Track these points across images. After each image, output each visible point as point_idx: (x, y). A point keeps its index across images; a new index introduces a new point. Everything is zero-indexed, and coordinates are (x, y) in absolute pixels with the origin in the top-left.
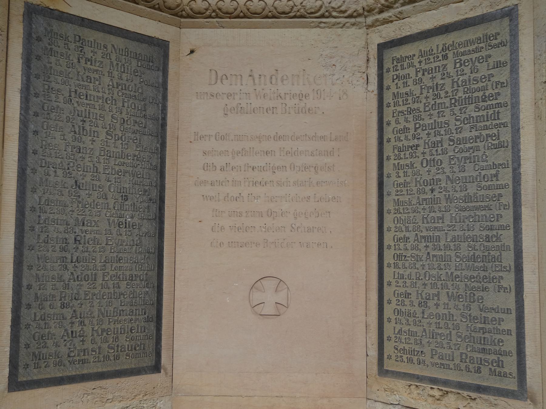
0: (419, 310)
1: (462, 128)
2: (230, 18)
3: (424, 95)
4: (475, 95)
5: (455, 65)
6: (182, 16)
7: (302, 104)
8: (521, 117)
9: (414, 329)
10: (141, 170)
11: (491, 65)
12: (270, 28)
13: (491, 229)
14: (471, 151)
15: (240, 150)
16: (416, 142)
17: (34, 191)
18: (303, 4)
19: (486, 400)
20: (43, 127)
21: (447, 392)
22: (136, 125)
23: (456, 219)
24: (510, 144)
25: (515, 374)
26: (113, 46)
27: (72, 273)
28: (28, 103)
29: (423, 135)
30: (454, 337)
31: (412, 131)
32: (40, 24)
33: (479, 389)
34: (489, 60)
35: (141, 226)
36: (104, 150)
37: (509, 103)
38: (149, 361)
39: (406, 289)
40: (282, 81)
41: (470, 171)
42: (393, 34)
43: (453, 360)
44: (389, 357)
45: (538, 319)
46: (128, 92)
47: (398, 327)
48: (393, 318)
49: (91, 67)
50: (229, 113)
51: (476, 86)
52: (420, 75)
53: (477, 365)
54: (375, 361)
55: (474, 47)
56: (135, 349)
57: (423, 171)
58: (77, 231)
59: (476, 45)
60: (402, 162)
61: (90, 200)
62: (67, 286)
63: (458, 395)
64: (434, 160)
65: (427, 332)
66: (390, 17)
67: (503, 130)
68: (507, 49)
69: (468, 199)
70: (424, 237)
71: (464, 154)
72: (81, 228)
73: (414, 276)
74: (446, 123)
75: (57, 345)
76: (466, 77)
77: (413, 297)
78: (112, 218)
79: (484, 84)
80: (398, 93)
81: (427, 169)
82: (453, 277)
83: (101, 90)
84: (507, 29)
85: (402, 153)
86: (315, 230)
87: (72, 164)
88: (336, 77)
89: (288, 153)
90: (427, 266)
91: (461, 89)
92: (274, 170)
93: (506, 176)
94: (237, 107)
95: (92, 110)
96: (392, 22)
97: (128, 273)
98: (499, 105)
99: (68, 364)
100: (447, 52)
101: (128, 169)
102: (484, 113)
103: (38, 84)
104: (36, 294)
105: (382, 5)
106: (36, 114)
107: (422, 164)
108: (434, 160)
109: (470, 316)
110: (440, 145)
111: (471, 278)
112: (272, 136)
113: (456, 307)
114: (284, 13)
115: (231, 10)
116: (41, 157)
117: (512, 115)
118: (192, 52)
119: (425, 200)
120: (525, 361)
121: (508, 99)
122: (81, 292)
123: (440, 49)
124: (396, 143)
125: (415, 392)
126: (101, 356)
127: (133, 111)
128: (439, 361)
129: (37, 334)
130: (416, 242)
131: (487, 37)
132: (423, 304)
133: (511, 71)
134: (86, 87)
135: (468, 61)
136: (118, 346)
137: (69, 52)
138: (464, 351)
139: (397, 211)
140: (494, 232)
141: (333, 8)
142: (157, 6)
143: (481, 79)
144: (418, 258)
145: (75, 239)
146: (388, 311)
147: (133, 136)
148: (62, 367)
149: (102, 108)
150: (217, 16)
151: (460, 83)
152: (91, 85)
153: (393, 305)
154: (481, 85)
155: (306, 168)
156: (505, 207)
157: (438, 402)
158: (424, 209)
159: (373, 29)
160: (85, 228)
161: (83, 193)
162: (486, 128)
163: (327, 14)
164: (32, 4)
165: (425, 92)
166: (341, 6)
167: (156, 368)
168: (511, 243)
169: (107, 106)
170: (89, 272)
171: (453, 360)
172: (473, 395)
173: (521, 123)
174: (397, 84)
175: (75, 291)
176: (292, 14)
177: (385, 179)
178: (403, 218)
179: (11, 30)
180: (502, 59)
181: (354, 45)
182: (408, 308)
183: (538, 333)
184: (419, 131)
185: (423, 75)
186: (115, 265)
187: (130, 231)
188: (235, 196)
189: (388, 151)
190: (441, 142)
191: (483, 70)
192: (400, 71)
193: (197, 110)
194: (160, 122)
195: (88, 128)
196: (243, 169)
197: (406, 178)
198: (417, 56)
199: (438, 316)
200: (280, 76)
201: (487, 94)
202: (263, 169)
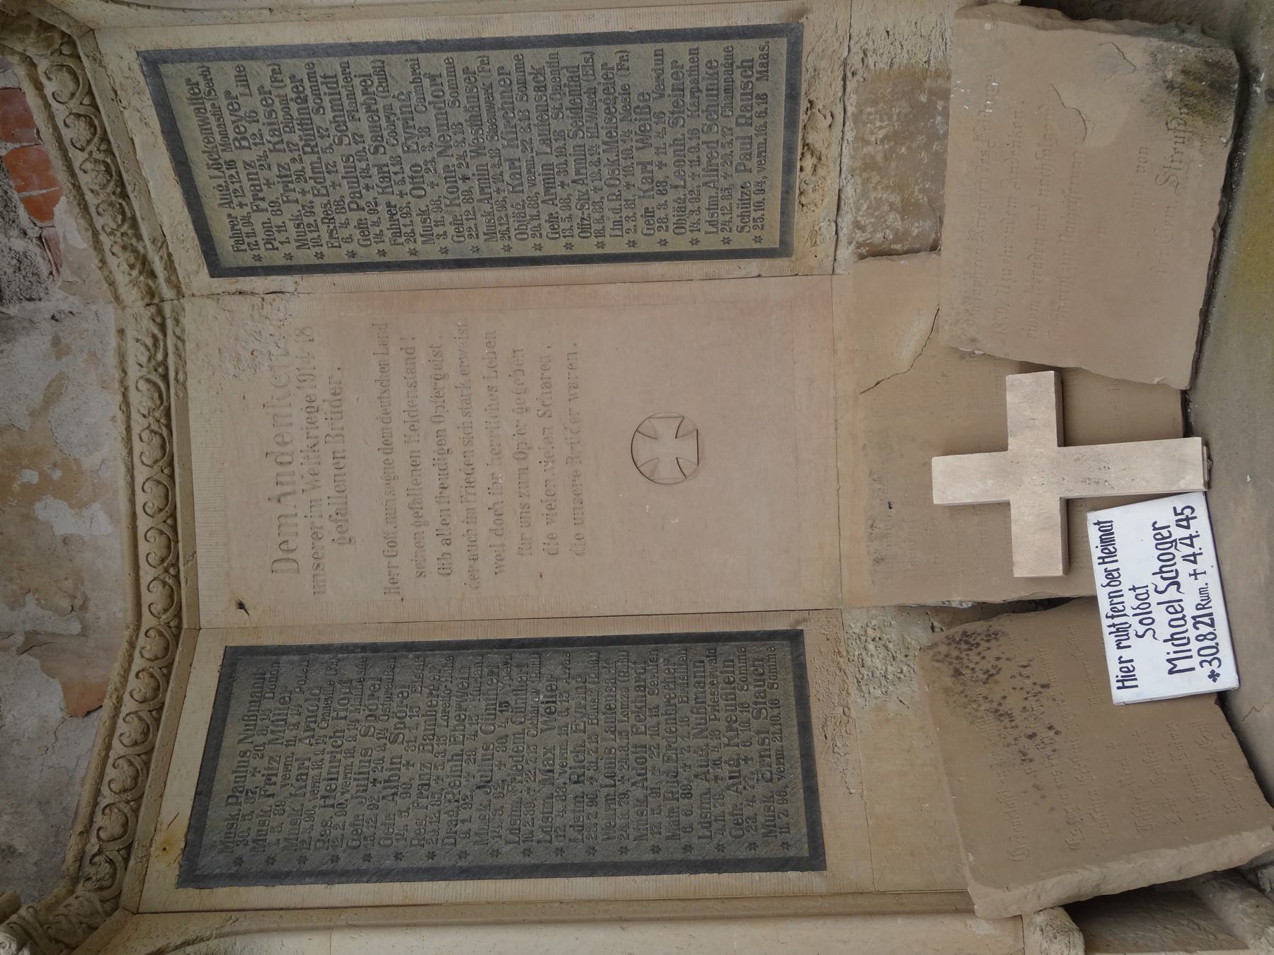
0: (672, 195)
1: (354, 134)
2: (177, 542)
3: (299, 196)
4: (295, 115)
5: (244, 148)
6: (179, 627)
7: (326, 406)
8: (331, 41)
9: (705, 202)
10: (455, 682)
11: (241, 90)
12: (191, 470)
13: (524, 84)
14: (392, 118)
15: (412, 512)
16: (382, 208)
17: (497, 853)
18: (146, 413)
19: (810, 85)
20: (388, 846)
21: (805, 145)
22: (376, 694)
23: (512, 140)
24: (378, 57)
25: (762, 42)
26: (240, 741)
27: (633, 784)
28: (348, 872)
29: (369, 196)
30: (712, 137)
31: (364, 215)
32: (211, 861)
33: (793, 96)
34: (233, 94)
35: (552, 677)
36: (423, 745)
37: (308, 60)
38: (783, 651)
39: (638, 216)
40: (287, 444)
41: (428, 118)
42: (191, 251)
43: (751, 138)
44: (758, 239)
45: (668, 9)
46: (320, 712)
47: (705, 227)
48: (690, 236)
49: (280, 775)
50: (347, 536)
51: (281, 114)
52: (263, 205)
53: (754, 101)
54: (768, 262)
55: (212, 119)
56: (762, 674)
57: (433, 194)
58: (562, 780)
59: (209, 115)
60: (419, 229)
61: (510, 763)
62: (655, 792)
63: (808, 128)
64: (412, 178)
65: (707, 179)
66: (161, 258)
67: (353, 69)
68: (214, 67)
70: (547, 190)
71: (400, 129)
72: (556, 775)
73: (616, 204)
74: (347, 160)
75: (753, 800)
76: (266, 130)
77: (651, 204)
78: (540, 725)
79: (277, 100)
80: (296, 241)
81: (428, 189)
82: (611, 142)
83: (320, 757)
84: (181, 66)
85: (404, 230)
86: (547, 374)
87: (449, 796)
88: (274, 350)
89: (413, 429)
90: (596, 183)
91: (286, 137)
93: (434, 63)
94: (336, 521)
95: (355, 769)
96: (170, 255)
97: (633, 694)
98: (312, 76)
99: (783, 781)
100: (222, 161)
101: (453, 704)
102: (327, 99)
104: (667, 838)
105: (141, 273)
106: (368, 858)
107: (420, 197)
108: (412, 178)
109: (673, 113)
110: (385, 169)
111: (610, 113)
112: (386, 457)
114: (163, 447)
115: (162, 541)
116: (439, 844)
117: (328, 55)
118: (241, 606)
119: (482, 190)
120: (737, 27)
122: (665, 767)
123: (216, 173)
124: (387, 240)
125: (812, 196)
126: (772, 729)
127: (352, 702)
128: (755, 160)
129: (734, 832)
130: (557, 202)
131: (195, 98)
132: (662, 188)
133: (252, 58)
134: (317, 781)
135: (238, 127)
136: (756, 703)
137: (257, 812)
138: (733, 120)
139: (505, 234)
140: (530, 78)
141: (149, 360)
142: (165, 671)
143: (268, 105)
144: (584, 198)
145: (576, 782)
146: (680, 244)
147: (397, 700)
148: (788, 790)
149: (351, 753)
150: (175, 564)
151: (276, 139)
152: (311, 773)
153: (668, 236)
154: (278, 106)
155: (438, 395)
156: (485, 62)
157: (824, 158)
158: (498, 191)
159: (183, 286)
160: (557, 769)
161: (498, 776)
162: (352, 95)
163: (160, 370)
164: (179, 876)
165: (293, 196)
166: (146, 346)
167: (794, 638)
168: (545, 53)
169: (347, 745)
170: (632, 757)
171: (751, 138)
172: (804, 105)
173: (341, 41)
174: (282, 243)
175: (664, 777)
176: (165, 432)
177: (450, 257)
178: (517, 224)
179: (228, 906)
180: (233, 73)
181: (216, 321)
182: (670, 211)
183: (690, 8)
184: (362, 203)
185: (263, 199)
186: (619, 717)
187: (561, 695)
188: (493, 518)
189: (401, 253)
190: (380, 167)
191: (255, 102)
192: (259, 239)
193: (345, 596)
194: (369, 654)
195: (386, 774)
196: (446, 506)
197: (447, 223)
198: (231, 211)
199: (679, 163)
200: (278, 449)
201: (294, 96)
202: (444, 472)
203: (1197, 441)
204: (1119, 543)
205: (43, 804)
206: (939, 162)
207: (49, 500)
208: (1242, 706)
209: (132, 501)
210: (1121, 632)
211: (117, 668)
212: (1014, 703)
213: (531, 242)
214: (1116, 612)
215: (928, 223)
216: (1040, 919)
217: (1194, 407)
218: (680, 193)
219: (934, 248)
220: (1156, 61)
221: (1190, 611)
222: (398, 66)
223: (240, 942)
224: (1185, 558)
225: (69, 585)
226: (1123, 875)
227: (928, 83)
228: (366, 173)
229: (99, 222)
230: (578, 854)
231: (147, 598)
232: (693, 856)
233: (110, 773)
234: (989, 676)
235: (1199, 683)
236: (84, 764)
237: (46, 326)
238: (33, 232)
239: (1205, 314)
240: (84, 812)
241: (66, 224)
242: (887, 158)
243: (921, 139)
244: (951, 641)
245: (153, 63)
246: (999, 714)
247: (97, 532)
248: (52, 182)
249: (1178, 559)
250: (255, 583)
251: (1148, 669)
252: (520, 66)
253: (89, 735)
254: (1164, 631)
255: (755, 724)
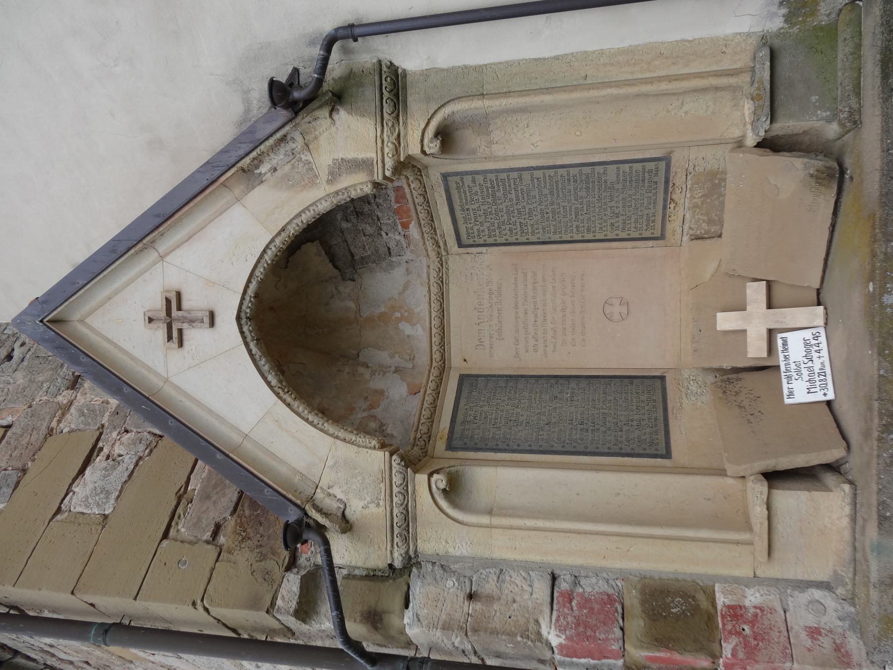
0: (621, 218)
9: (633, 220)
29: (513, 219)
32: (456, 443)
33: (667, 182)
38: (658, 383)
41: (536, 193)
44: (652, 233)
47: (633, 229)
60: (530, 231)
62: (609, 429)
68: (465, 177)
69: (552, 193)
77: (613, 221)
82: (600, 199)
92: (536, 308)
103: (491, 444)
106: (508, 445)
113: (617, 197)
121: (494, 175)
131: (458, 188)
134: (491, 420)
139: (560, 232)
155: (535, 289)
161: (553, 420)
162: (510, 186)
167: (662, 378)
172: (671, 185)
181: (460, 263)
191: (477, 189)
193: (501, 357)
199: (624, 207)
203: (822, 308)
204: (789, 343)
205: (402, 422)
206: (722, 204)
207: (403, 322)
208: (836, 406)
209: (431, 323)
210: (789, 378)
211: (425, 379)
212: (746, 403)
213: (569, 235)
214: (787, 371)
215: (718, 227)
216: (752, 478)
217: (821, 295)
218: (624, 217)
219: (720, 236)
220: (806, 167)
221: (817, 371)
222: (526, 175)
223: (467, 468)
224: (816, 351)
225: (409, 351)
226: (785, 463)
227: (718, 176)
228: (513, 212)
229: (424, 230)
230: (581, 449)
231: (434, 356)
232: (623, 451)
233: (424, 412)
234: (737, 393)
235: (819, 397)
236: (415, 410)
237: (404, 265)
238: (402, 233)
239: (826, 260)
240: (416, 424)
241: (414, 231)
242: (702, 204)
243: (715, 196)
244: (722, 381)
245: (445, 176)
246: (740, 407)
247: (418, 333)
248: (409, 216)
249: (813, 352)
250: (471, 352)
251: (799, 391)
252: (568, 174)
253: (416, 400)
254: (806, 377)
255: (647, 408)
